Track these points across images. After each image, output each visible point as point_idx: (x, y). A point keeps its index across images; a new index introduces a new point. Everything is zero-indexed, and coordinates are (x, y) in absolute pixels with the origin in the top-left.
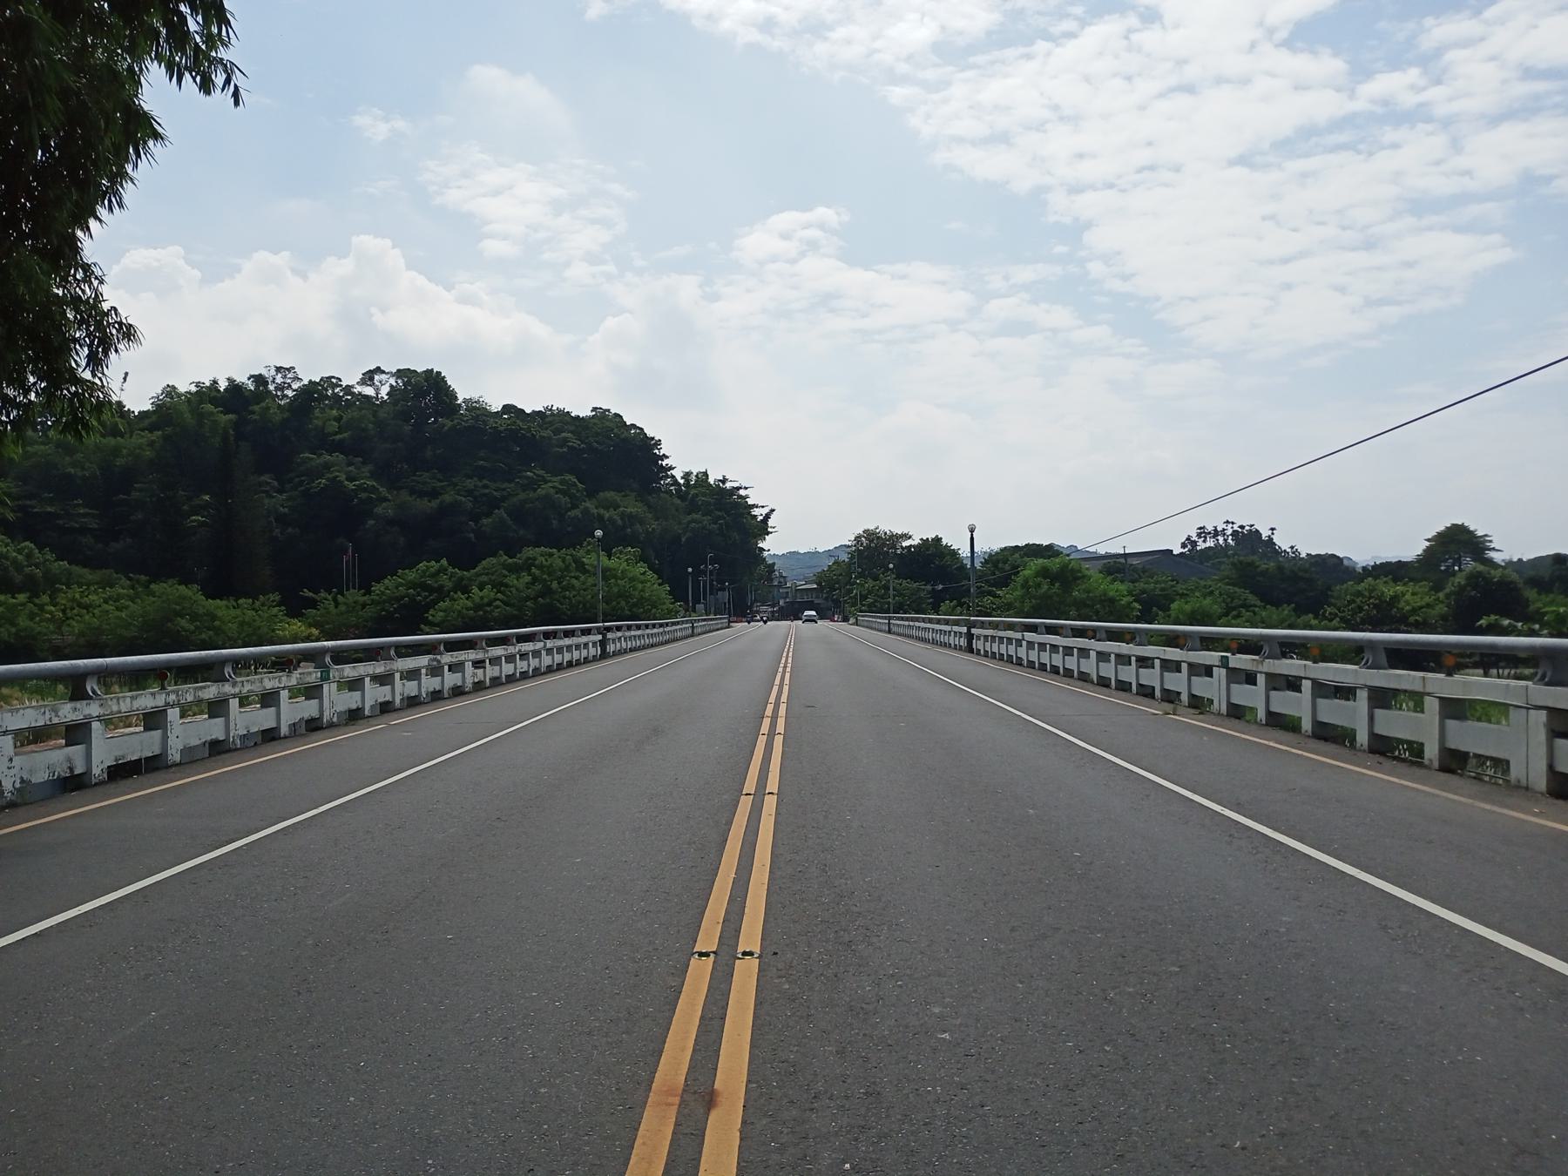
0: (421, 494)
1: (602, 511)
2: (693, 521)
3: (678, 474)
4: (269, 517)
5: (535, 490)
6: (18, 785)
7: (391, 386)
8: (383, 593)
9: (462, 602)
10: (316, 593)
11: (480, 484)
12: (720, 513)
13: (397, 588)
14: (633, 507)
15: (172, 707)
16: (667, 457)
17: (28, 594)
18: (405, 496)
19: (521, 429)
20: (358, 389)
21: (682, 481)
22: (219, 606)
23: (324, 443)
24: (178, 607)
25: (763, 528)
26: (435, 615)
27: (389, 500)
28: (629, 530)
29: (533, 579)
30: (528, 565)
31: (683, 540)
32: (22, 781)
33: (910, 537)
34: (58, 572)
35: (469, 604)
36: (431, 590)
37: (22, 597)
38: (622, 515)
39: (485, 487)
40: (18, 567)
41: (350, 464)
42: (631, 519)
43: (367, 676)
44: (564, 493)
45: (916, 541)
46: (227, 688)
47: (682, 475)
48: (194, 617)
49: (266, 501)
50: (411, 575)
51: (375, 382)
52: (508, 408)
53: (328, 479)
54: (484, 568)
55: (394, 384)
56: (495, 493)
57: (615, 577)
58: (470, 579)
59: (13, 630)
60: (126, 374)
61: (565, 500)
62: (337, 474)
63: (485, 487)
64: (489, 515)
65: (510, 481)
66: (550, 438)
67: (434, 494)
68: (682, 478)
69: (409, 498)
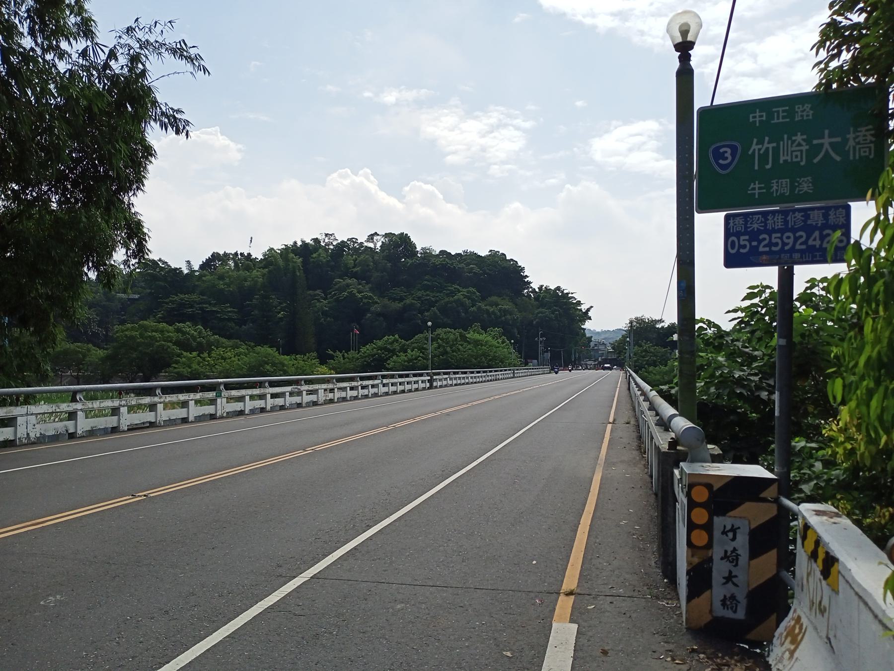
0: (394, 300)
1: (488, 307)
3: (535, 286)
6: (38, 435)
9: (403, 357)
10: (335, 352)
11: (425, 294)
14: (507, 305)
15: (123, 406)
16: (528, 277)
17: (198, 352)
20: (365, 244)
22: (285, 358)
24: (266, 359)
25: (585, 316)
27: (379, 304)
32: (41, 434)
33: (663, 322)
35: (406, 359)
37: (195, 354)
38: (500, 310)
39: (427, 295)
40: (194, 338)
41: (360, 284)
42: (505, 312)
43: (248, 395)
44: (469, 298)
45: (666, 325)
46: (156, 399)
48: (274, 364)
49: (318, 304)
50: (380, 343)
53: (348, 292)
54: (416, 340)
57: (482, 345)
59: (190, 370)
60: (252, 238)
61: (467, 302)
63: (427, 295)
64: (428, 311)
65: (441, 292)
66: (463, 268)
69: (388, 302)
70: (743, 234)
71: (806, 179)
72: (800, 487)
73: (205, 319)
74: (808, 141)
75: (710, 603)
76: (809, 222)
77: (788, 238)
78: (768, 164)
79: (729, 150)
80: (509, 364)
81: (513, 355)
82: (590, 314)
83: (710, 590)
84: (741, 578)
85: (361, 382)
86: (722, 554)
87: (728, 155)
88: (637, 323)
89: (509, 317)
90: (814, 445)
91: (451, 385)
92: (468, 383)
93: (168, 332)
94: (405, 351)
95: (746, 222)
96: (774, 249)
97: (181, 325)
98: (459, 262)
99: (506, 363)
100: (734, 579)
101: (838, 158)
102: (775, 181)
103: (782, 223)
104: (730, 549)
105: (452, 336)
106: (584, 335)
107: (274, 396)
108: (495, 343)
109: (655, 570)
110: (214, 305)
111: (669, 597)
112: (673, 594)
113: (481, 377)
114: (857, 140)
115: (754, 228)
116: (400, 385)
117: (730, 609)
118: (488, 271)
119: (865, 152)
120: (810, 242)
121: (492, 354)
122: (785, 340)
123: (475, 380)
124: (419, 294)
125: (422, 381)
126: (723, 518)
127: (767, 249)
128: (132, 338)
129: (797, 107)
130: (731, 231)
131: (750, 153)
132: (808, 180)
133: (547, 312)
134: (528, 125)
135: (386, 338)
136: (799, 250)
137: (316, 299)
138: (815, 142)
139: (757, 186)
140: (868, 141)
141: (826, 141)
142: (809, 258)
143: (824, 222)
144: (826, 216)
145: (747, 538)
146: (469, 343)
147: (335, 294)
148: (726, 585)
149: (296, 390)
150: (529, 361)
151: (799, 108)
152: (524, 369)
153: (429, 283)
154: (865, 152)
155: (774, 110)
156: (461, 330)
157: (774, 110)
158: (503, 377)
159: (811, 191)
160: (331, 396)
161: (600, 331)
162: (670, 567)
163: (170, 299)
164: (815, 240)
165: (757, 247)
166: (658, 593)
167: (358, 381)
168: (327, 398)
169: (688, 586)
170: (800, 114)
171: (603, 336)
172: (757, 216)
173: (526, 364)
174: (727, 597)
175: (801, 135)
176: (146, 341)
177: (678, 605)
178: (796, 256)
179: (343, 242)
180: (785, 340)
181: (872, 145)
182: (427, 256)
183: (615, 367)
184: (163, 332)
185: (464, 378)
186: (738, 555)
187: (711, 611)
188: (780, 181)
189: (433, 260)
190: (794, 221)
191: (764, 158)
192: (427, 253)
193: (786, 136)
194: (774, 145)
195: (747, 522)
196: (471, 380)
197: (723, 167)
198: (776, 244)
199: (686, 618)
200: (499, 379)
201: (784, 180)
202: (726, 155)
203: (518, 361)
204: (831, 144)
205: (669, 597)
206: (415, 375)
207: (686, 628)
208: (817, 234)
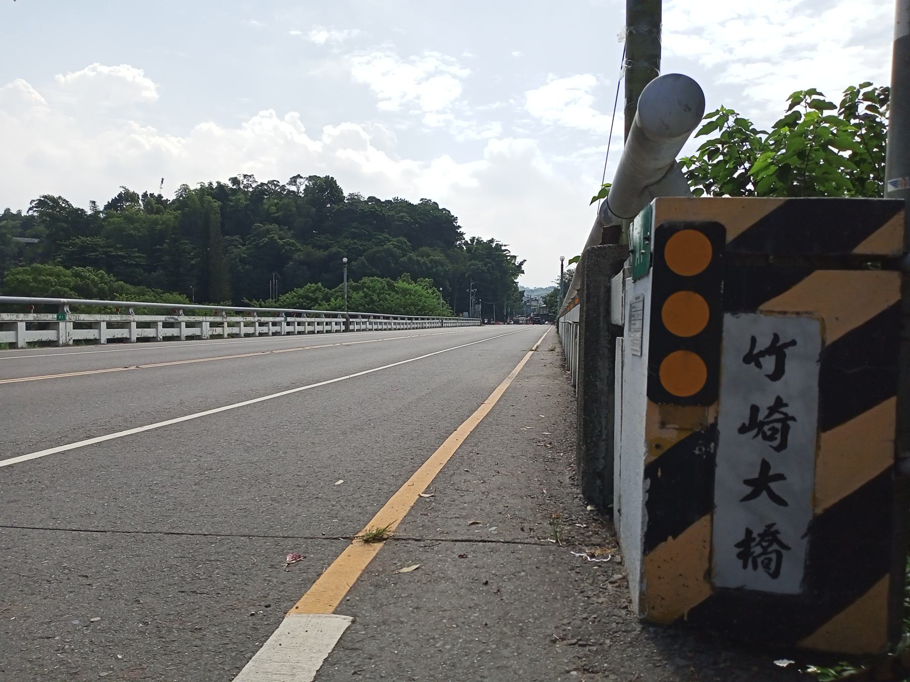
1: (419, 258)
4: (236, 259)
7: (306, 185)
8: (285, 301)
11: (352, 242)
13: (293, 298)
14: (438, 256)
18: (310, 248)
19: (377, 210)
20: (288, 187)
23: (269, 218)
25: (519, 270)
28: (435, 270)
29: (365, 295)
31: (466, 275)
34: (116, 286)
38: (431, 261)
39: (355, 243)
40: (95, 284)
41: (281, 230)
42: (436, 263)
50: (301, 291)
51: (297, 183)
52: (371, 199)
53: (269, 238)
54: (340, 288)
55: (308, 184)
56: (360, 248)
57: (410, 294)
58: (332, 294)
60: (163, 179)
62: (273, 235)
63: (355, 243)
65: (369, 241)
66: (393, 216)
67: (326, 247)
69: (311, 250)
73: (109, 264)
75: (707, 552)
81: (446, 309)
82: (523, 267)
83: (708, 517)
85: (259, 318)
86: (744, 417)
88: (569, 275)
89: (440, 268)
93: (65, 276)
94: (328, 300)
97: (80, 269)
100: (773, 485)
104: (765, 402)
105: (379, 285)
106: (517, 288)
107: (140, 325)
108: (424, 293)
109: (569, 490)
110: (121, 249)
111: (596, 540)
112: (604, 533)
113: (406, 323)
117: (760, 568)
121: (421, 303)
123: (398, 327)
124: (347, 242)
126: (752, 315)
128: (23, 282)
133: (480, 264)
134: (465, 73)
135: (307, 286)
145: (815, 369)
146: (397, 292)
147: (254, 240)
148: (753, 502)
149: (173, 320)
152: (453, 319)
156: (388, 279)
158: (430, 325)
161: (533, 288)
162: (598, 482)
163: (70, 241)
166: (573, 533)
167: (254, 316)
168: (214, 333)
169: (650, 505)
171: (536, 293)
174: (755, 535)
176: (40, 286)
177: (618, 558)
179: (262, 184)
182: (355, 202)
183: (547, 322)
184: (59, 276)
185: (385, 323)
192: (355, 199)
195: (815, 327)
196: (395, 327)
199: (642, 594)
205: (596, 540)
207: (641, 621)
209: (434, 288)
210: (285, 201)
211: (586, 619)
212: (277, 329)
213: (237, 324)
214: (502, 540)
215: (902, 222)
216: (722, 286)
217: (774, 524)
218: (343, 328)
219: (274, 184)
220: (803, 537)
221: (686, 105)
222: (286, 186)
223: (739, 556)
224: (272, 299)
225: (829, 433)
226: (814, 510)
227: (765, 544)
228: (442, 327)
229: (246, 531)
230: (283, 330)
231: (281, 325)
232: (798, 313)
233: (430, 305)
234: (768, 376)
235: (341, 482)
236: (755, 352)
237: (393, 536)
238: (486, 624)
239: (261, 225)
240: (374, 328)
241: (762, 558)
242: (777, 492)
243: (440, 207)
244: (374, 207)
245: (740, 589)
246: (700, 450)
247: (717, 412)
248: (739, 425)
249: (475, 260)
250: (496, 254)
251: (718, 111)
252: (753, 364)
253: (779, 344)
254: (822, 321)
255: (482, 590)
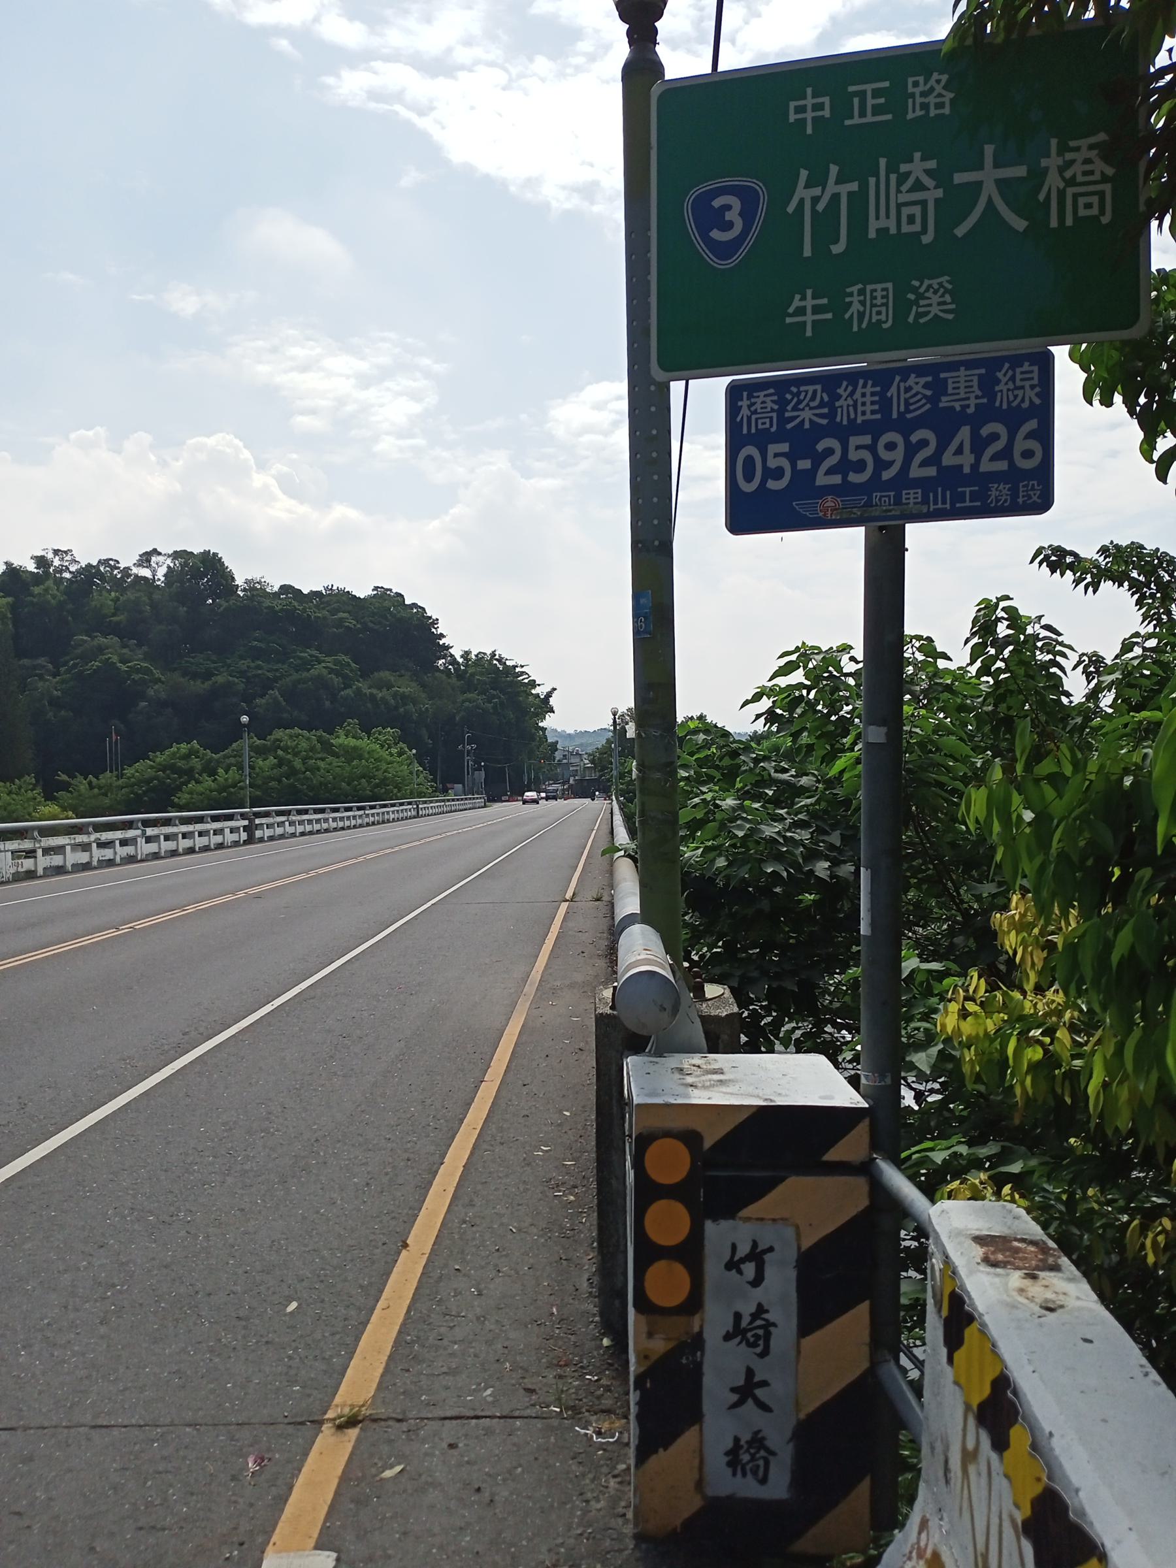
0: (194, 676)
1: (374, 691)
2: (469, 701)
3: (457, 653)
5: (309, 670)
7: (169, 567)
10: (73, 777)
11: (252, 665)
12: (495, 693)
14: (407, 687)
20: (135, 570)
21: (461, 660)
25: (544, 706)
26: (183, 797)
27: (163, 683)
30: (277, 744)
36: (180, 772)
38: (395, 696)
39: (259, 667)
41: (124, 646)
42: (404, 699)
44: (338, 673)
47: (461, 653)
49: (40, 684)
50: (160, 758)
51: (152, 563)
52: (286, 589)
55: (172, 565)
57: (360, 758)
58: (218, 761)
61: (336, 680)
63: (259, 667)
64: (262, 696)
66: (325, 618)
67: (208, 675)
68: (462, 656)
69: (182, 679)
70: (777, 438)
71: (935, 283)
72: (908, 1059)
74: (940, 177)
75: (696, 1462)
76: (944, 402)
77: (891, 446)
78: (836, 241)
79: (735, 203)
80: (411, 793)
81: (419, 776)
82: (552, 701)
83: (696, 1427)
84: (778, 1390)
85: (98, 835)
86: (729, 1327)
87: (733, 215)
89: (411, 707)
90: (935, 966)
91: (293, 835)
92: (327, 831)
94: (213, 773)
95: (782, 404)
96: (854, 478)
98: (317, 606)
99: (406, 790)
100: (759, 1392)
101: (1020, 225)
102: (855, 289)
103: (876, 407)
104: (747, 1309)
108: (384, 754)
113: (354, 817)
114: (1068, 174)
115: (803, 421)
116: (215, 834)
117: (749, 1476)
118: (371, 625)
119: (1088, 206)
120: (948, 459)
121: (379, 774)
122: (884, 730)
123: (341, 824)
124: (243, 664)
125: (232, 829)
127: (837, 479)
129: (910, 80)
130: (745, 431)
131: (790, 209)
132: (941, 285)
136: (919, 479)
137: (36, 675)
138: (959, 178)
139: (809, 303)
140: (1097, 177)
141: (988, 176)
142: (944, 502)
143: (985, 400)
144: (988, 385)
145: (792, 1274)
147: (75, 665)
148: (739, 1410)
150: (449, 785)
151: (916, 84)
152: (437, 801)
153: (259, 644)
154: (1088, 206)
155: (851, 89)
156: (320, 732)
157: (851, 89)
159: (950, 317)
160: (28, 864)
164: (959, 451)
165: (813, 471)
167: (88, 833)
168: (20, 869)
170: (919, 100)
171: (578, 741)
172: (811, 388)
173: (445, 791)
174: (742, 1442)
175: (923, 159)
178: (912, 497)
179: (89, 566)
180: (884, 730)
181: (1107, 188)
185: (318, 821)
186: (769, 1325)
187: (699, 1485)
188: (869, 287)
189: (267, 603)
190: (906, 400)
191: (826, 223)
193: (883, 162)
194: (854, 186)
195: (790, 1232)
196: (334, 825)
197: (724, 250)
198: (860, 466)
200: (388, 821)
201: (879, 286)
202: (728, 216)
203: (428, 787)
204: (1001, 183)
206: (215, 819)
208: (965, 433)
209: (401, 744)
210: (130, 595)
211: (581, 1535)
212: (129, 850)
213: (60, 850)
214: (498, 1414)
215: (867, 1129)
216: (702, 1194)
217: (759, 1431)
218: (244, 836)
219: (110, 566)
220: (788, 1443)
221: (661, 1006)
222: (133, 568)
223: (729, 1464)
224: (111, 771)
225: (808, 1338)
226: (797, 1414)
227: (752, 1451)
228: (417, 816)
229: (189, 1416)
230: (139, 852)
231: (135, 844)
232: (774, 1220)
233: (395, 776)
234: (749, 1283)
235: (294, 1305)
236: (736, 1258)
237: (371, 1415)
238: (477, 1553)
239: (85, 638)
240: (298, 831)
241: (750, 1465)
242: (762, 1399)
243: (407, 602)
244: (291, 603)
245: (730, 1498)
246: (687, 1359)
247: (702, 1320)
248: (724, 1332)
249: (470, 692)
250: (506, 681)
251: (797, 649)
252: (734, 1271)
253: (758, 1250)
254: (797, 1227)
255: (474, 1501)
